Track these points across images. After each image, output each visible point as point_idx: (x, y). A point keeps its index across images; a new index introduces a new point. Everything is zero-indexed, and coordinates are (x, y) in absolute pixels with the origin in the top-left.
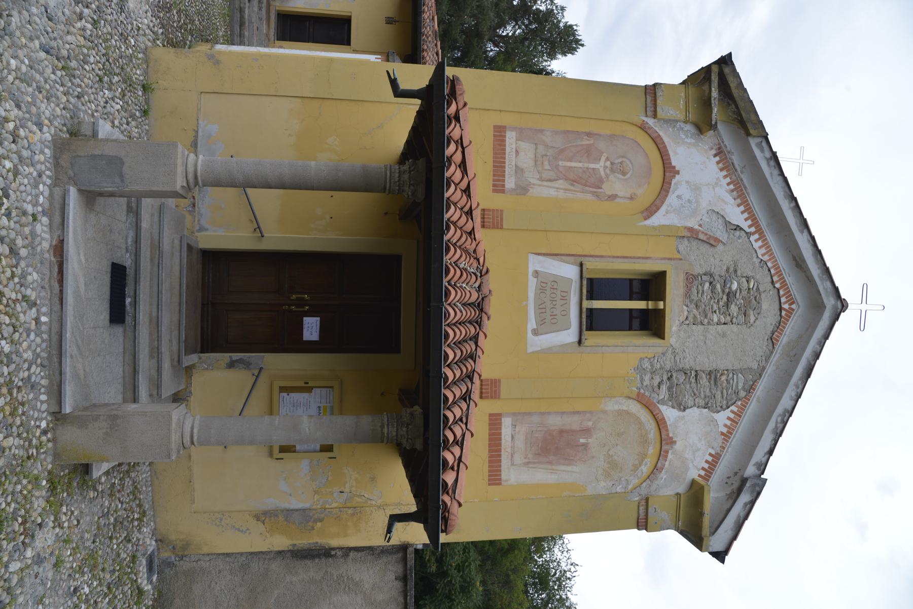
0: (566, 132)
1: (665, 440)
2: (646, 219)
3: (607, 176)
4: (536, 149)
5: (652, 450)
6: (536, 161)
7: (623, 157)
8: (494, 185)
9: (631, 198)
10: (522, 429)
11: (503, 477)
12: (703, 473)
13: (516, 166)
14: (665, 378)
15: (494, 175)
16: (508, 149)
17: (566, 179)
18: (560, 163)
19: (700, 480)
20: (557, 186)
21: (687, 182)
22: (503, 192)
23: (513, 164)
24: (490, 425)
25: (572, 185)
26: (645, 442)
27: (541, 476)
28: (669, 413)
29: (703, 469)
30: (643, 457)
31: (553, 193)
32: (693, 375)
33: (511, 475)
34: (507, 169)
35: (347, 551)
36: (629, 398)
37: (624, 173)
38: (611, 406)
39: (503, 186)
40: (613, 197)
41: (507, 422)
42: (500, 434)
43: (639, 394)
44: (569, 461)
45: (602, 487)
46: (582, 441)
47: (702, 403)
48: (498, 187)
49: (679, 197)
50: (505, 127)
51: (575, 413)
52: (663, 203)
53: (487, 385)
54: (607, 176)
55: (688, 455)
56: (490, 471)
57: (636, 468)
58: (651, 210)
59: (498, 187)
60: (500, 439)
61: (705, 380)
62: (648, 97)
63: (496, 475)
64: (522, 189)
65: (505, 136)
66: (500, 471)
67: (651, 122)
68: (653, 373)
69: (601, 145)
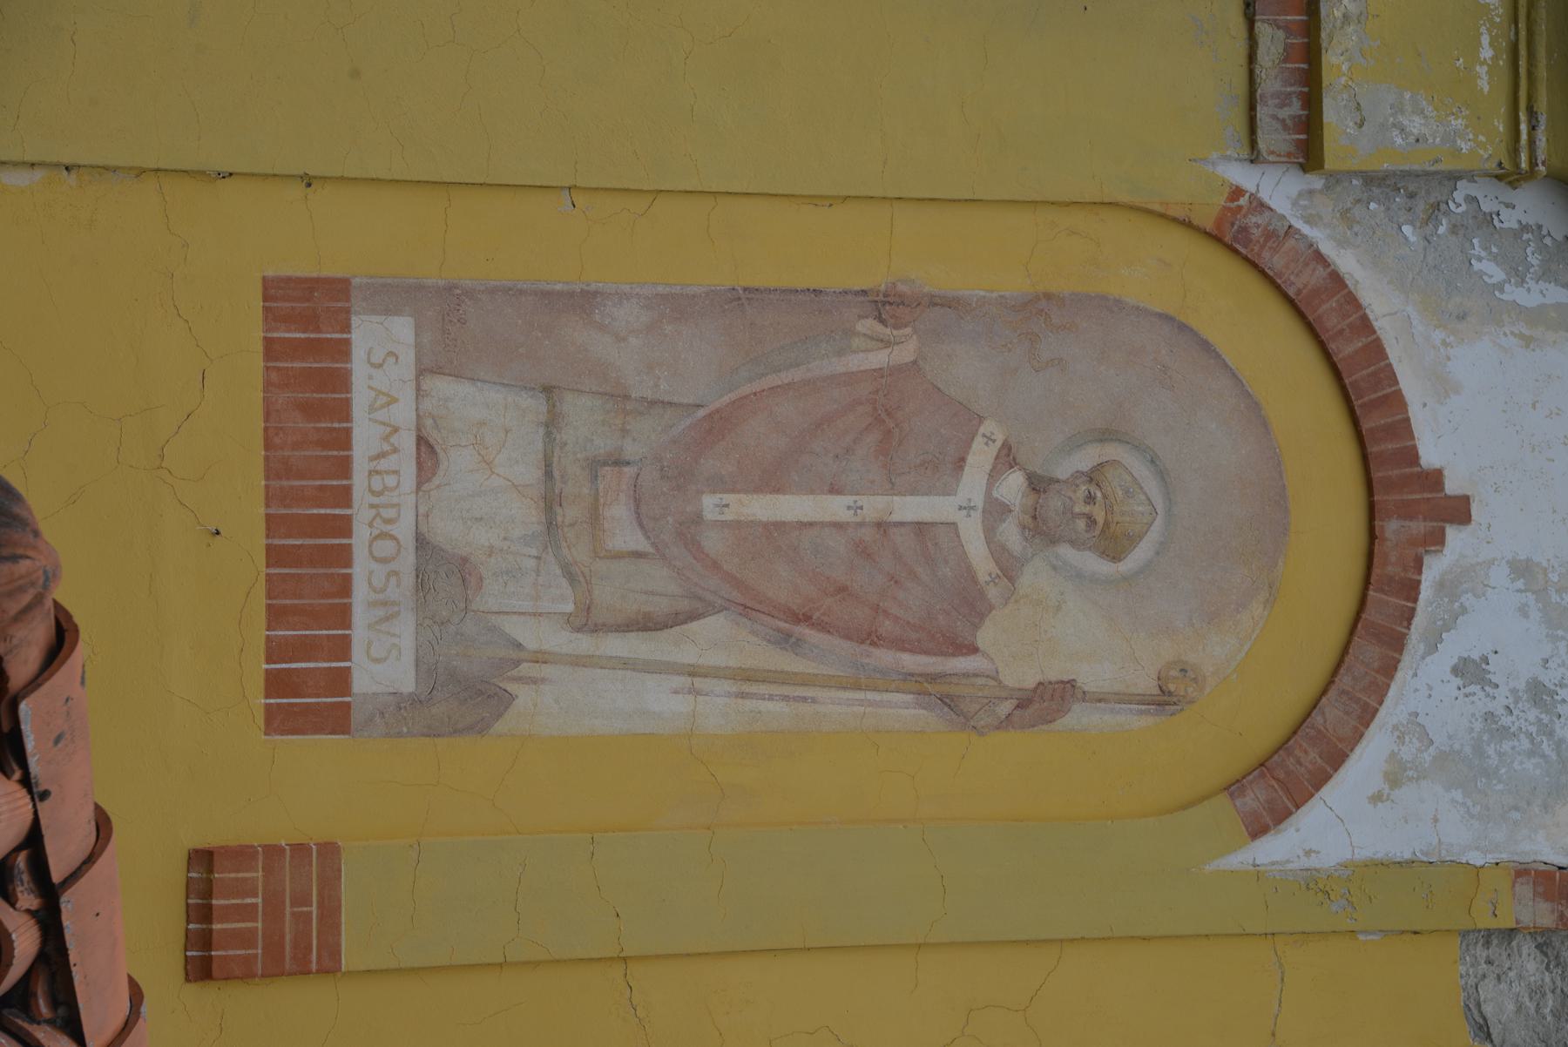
0: (745, 298)
2: (1258, 830)
3: (1008, 569)
4: (552, 423)
6: (550, 503)
7: (1106, 436)
8: (276, 684)
9: (1164, 700)
13: (422, 542)
15: (276, 615)
16: (364, 436)
17: (749, 607)
18: (709, 502)
20: (688, 655)
21: (1523, 570)
22: (337, 720)
23: (404, 530)
25: (786, 641)
31: (663, 702)
34: (361, 569)
37: (1113, 543)
39: (341, 682)
40: (1047, 701)
48: (306, 693)
49: (1471, 671)
50: (339, 288)
52: (1367, 716)
54: (1008, 569)
58: (1286, 775)
59: (306, 693)
62: (1264, 30)
64: (467, 696)
65: (342, 350)
67: (1280, 191)
69: (965, 368)
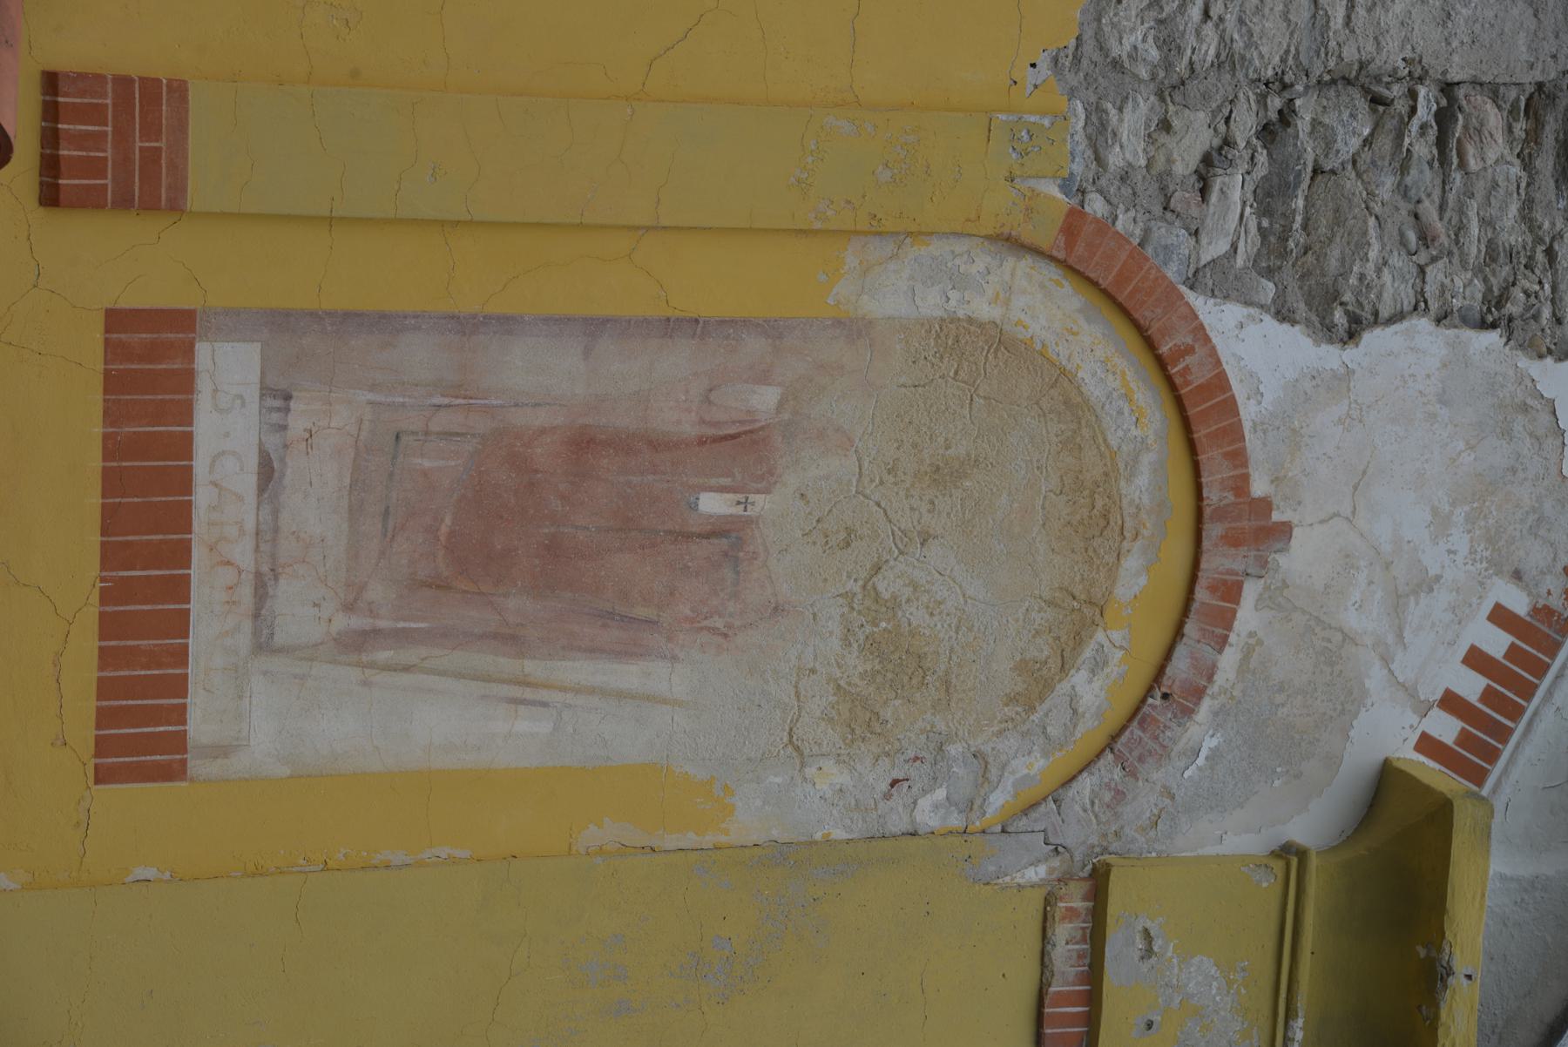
1: (1224, 522)
5: (1141, 578)
10: (331, 421)
11: (200, 725)
12: (1446, 728)
14: (1245, 124)
19: (1430, 771)
24: (112, 382)
26: (1097, 524)
27: (446, 719)
28: (1258, 350)
29: (1451, 702)
30: (1082, 614)
32: (1425, 111)
33: (252, 711)
36: (1014, 244)
38: (899, 291)
41: (227, 373)
42: (184, 445)
43: (1074, 222)
44: (628, 629)
45: (826, 796)
46: (713, 504)
47: (1468, 292)
51: (670, 327)
53: (94, 113)
55: (1361, 616)
56: (105, 689)
57: (1036, 683)
60: (184, 482)
61: (1498, 147)
63: (154, 715)
66: (179, 686)
68: (1170, 90)
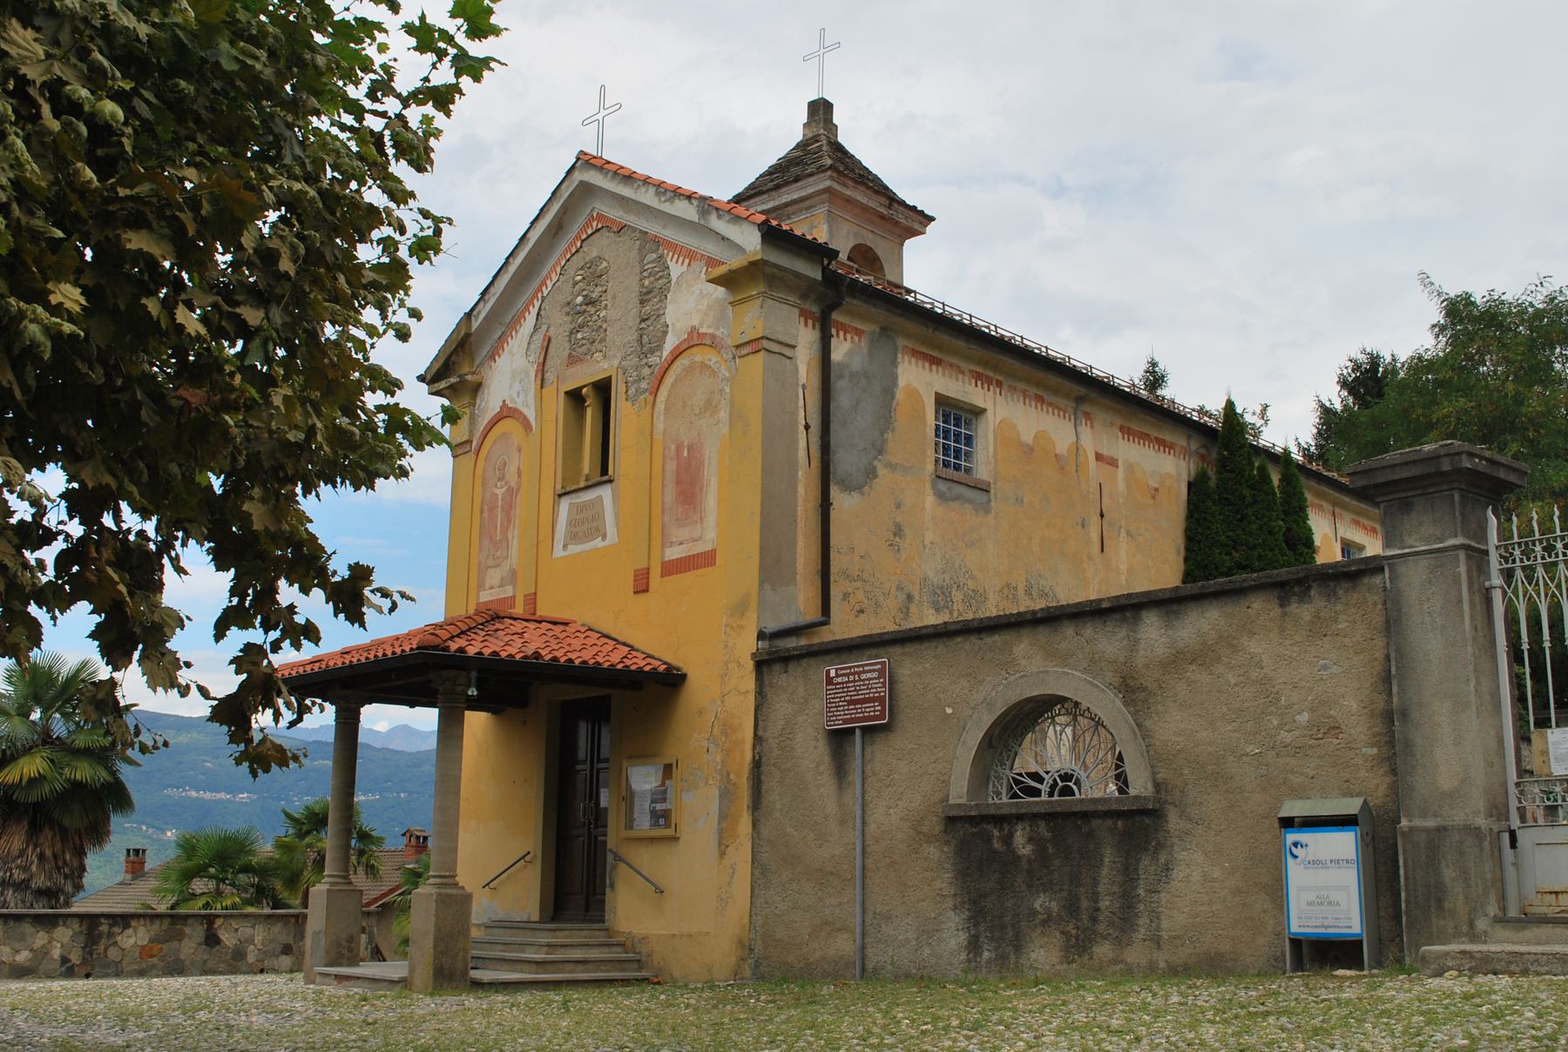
35: (758, 739)
58: (526, 425)
